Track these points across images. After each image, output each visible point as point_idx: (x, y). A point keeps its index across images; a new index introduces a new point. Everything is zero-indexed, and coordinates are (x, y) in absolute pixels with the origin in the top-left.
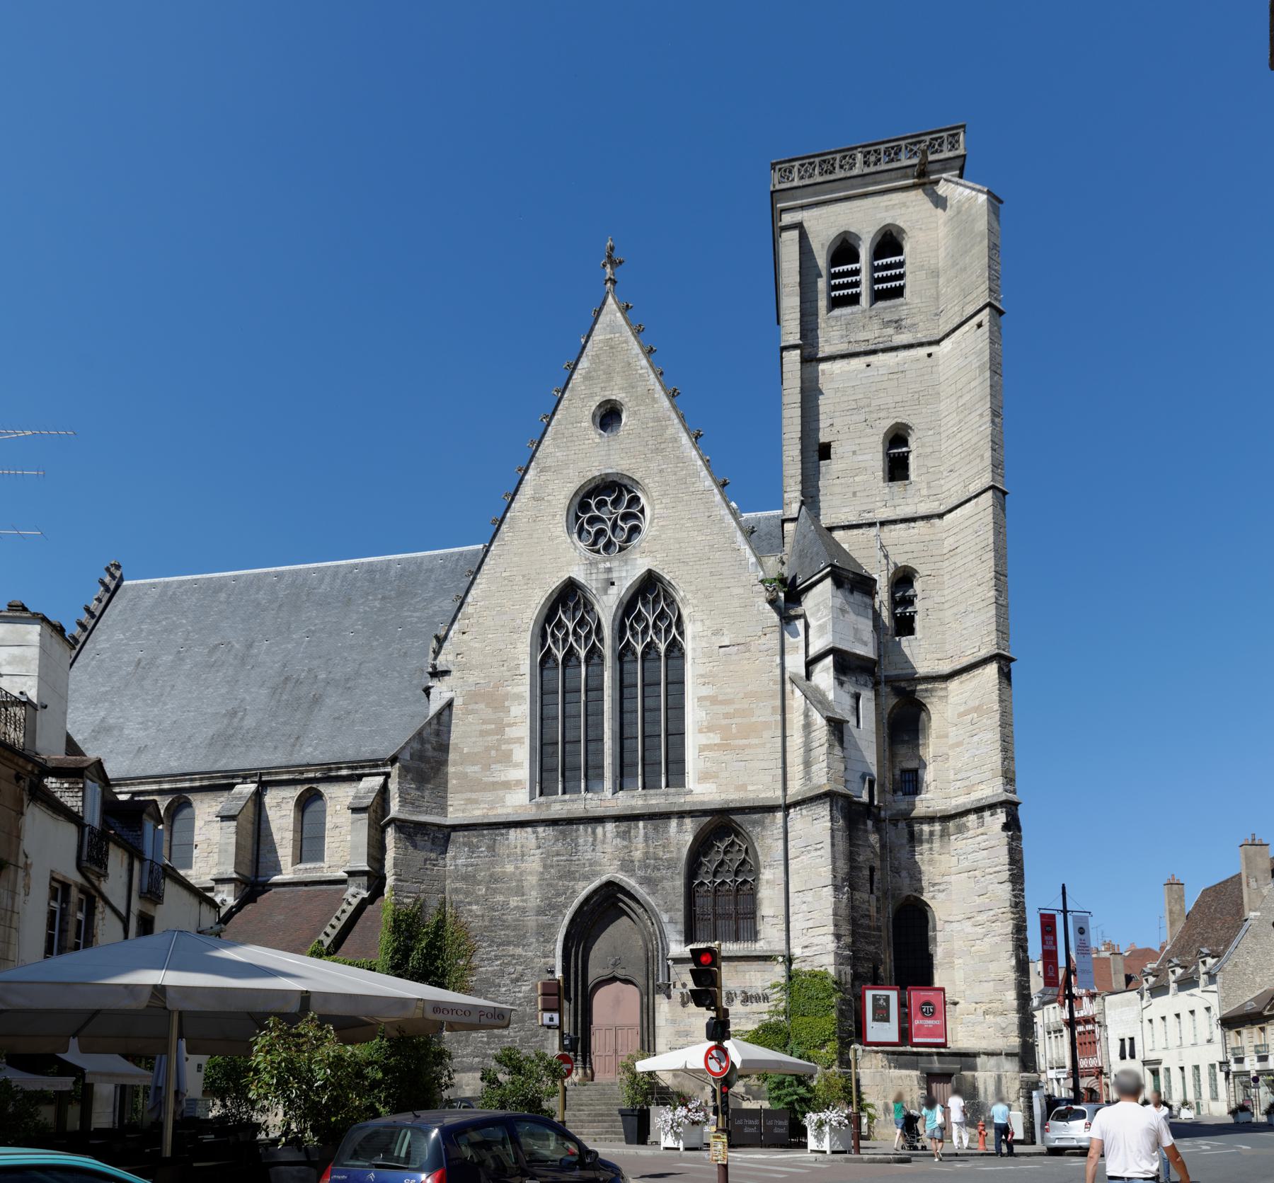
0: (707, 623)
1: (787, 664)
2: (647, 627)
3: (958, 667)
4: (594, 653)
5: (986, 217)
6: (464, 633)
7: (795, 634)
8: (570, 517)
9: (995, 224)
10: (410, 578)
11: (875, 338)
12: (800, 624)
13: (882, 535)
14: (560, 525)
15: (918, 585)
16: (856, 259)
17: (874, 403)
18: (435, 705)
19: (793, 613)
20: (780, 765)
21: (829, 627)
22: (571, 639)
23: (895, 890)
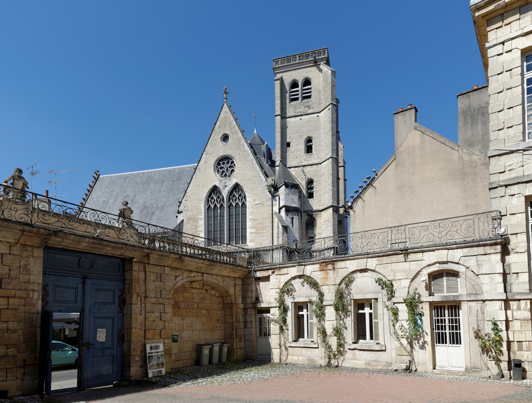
0: (252, 198)
1: (274, 209)
2: (236, 198)
3: (324, 208)
4: (221, 206)
7: (276, 201)
9: (334, 79)
10: (181, 173)
12: (277, 198)
13: (304, 170)
15: (314, 183)
16: (298, 86)
17: (302, 130)
18: (179, 222)
19: (275, 195)
20: (271, 238)
21: (284, 199)
22: (216, 202)
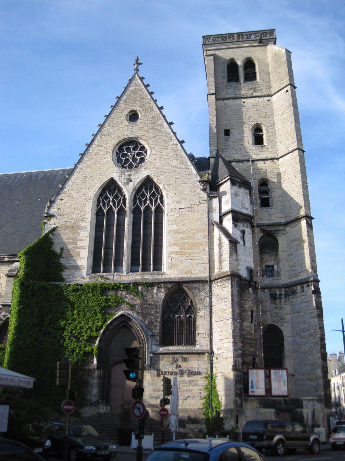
5: (286, 57)
6: (62, 200)
8: (114, 153)
11: (246, 93)
14: (109, 156)
22: (111, 203)
23: (264, 321)
